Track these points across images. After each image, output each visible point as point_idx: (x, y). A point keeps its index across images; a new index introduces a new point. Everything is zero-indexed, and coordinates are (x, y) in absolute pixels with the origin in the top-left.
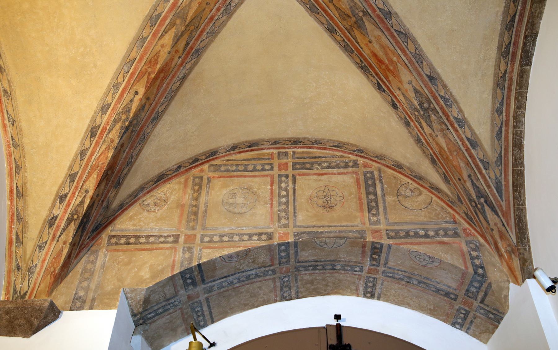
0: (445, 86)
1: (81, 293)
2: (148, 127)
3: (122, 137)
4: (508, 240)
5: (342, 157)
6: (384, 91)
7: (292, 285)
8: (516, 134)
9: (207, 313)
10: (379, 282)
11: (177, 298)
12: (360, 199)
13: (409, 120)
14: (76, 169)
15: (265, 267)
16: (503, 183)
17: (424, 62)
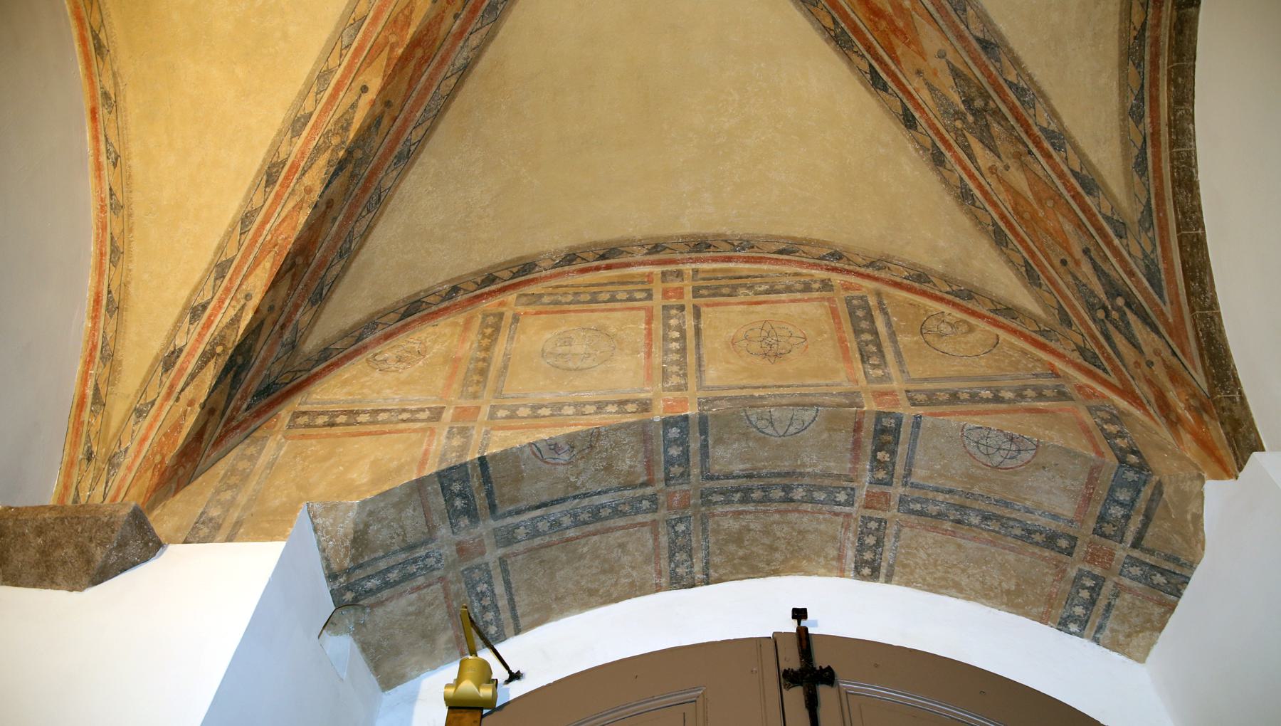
0: (1016, 62)
1: (214, 512)
2: (387, 174)
3: (330, 182)
4: (1189, 385)
5: (796, 274)
6: (885, 88)
7: (694, 545)
8: (1178, 159)
9: (503, 603)
10: (891, 530)
11: (432, 546)
12: (842, 341)
13: (943, 149)
14: (231, 251)
15: (634, 487)
16: (1162, 266)
17: (968, 8)
